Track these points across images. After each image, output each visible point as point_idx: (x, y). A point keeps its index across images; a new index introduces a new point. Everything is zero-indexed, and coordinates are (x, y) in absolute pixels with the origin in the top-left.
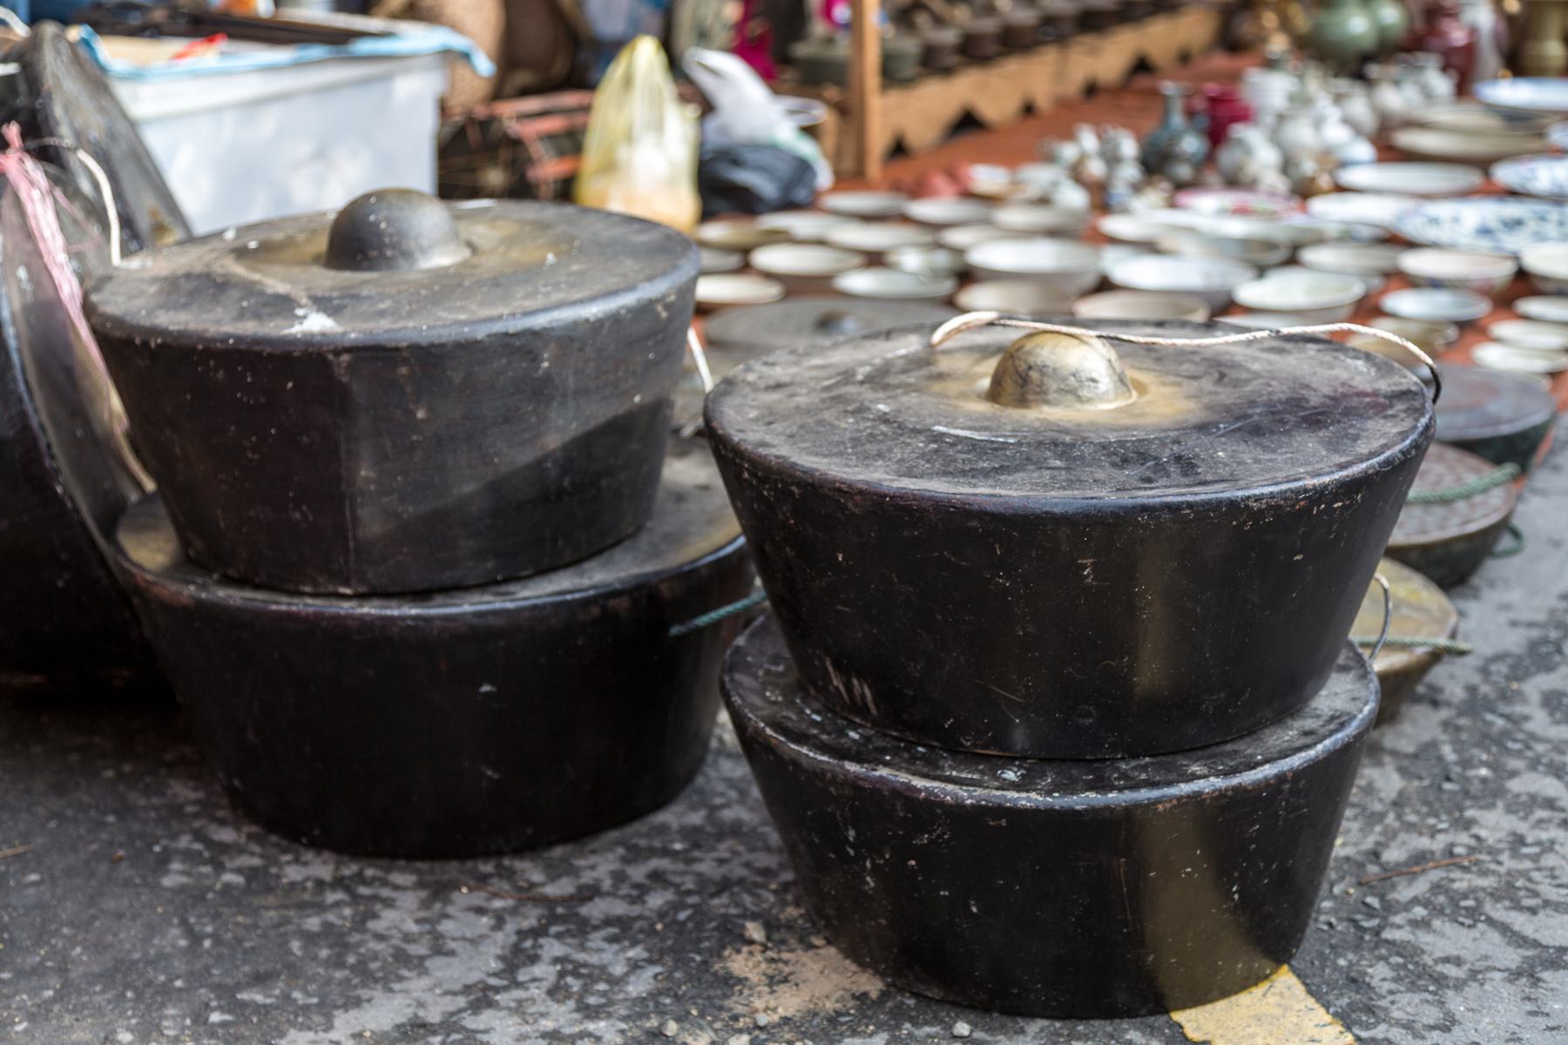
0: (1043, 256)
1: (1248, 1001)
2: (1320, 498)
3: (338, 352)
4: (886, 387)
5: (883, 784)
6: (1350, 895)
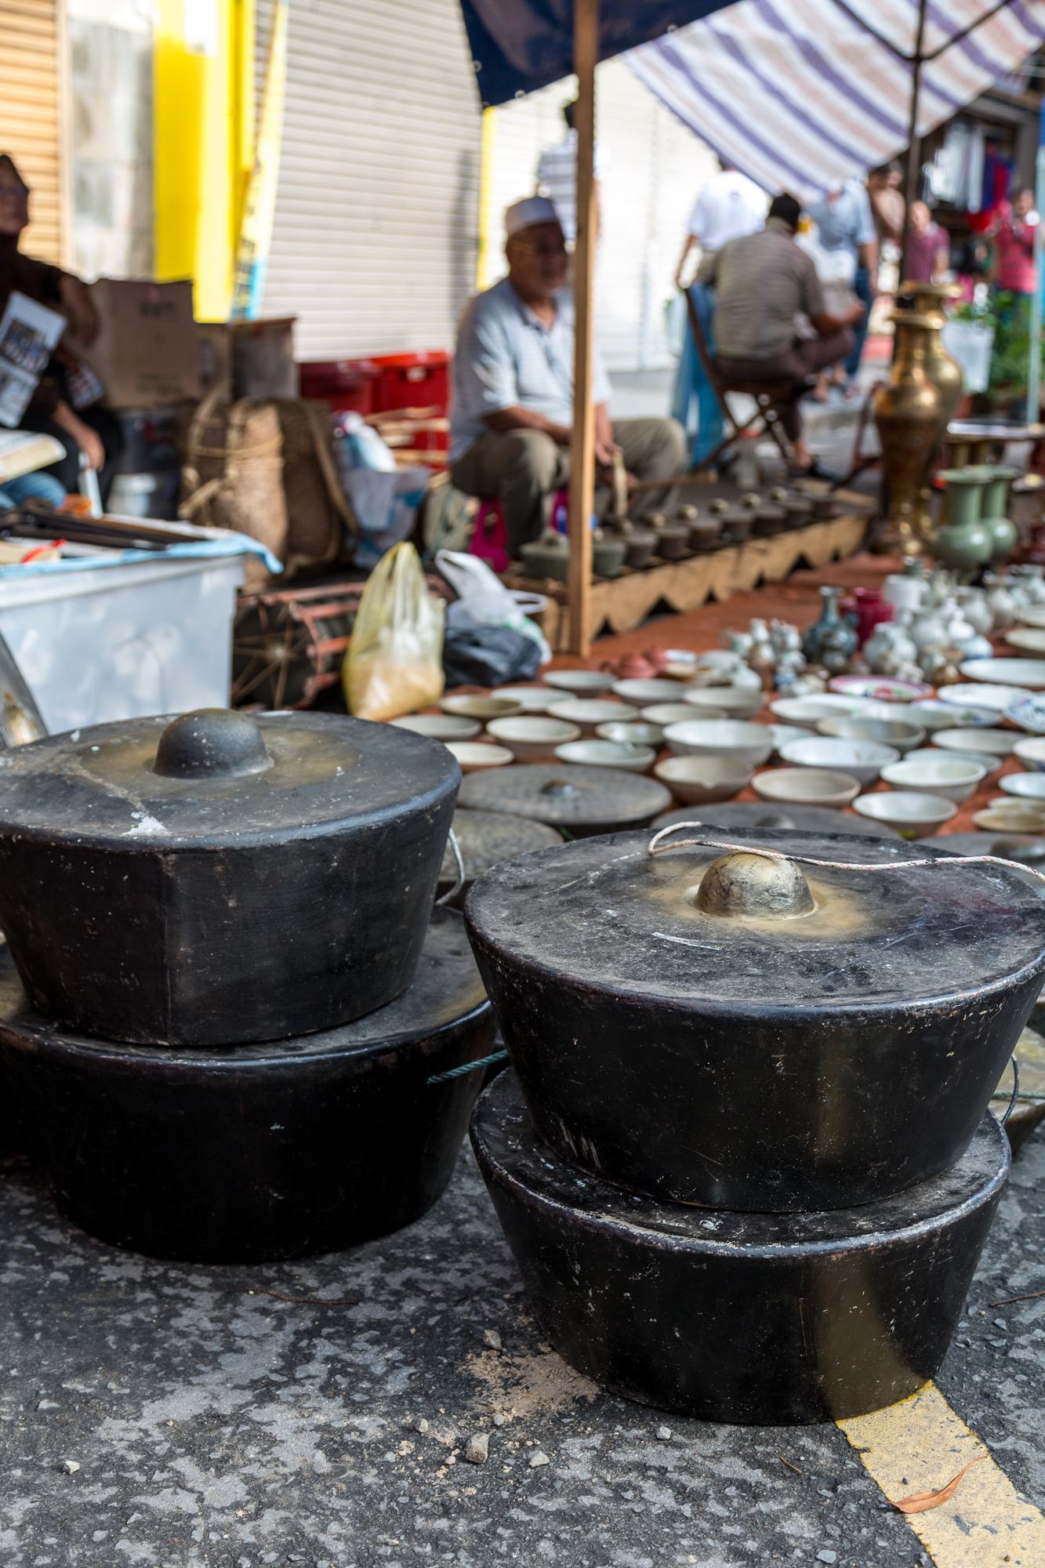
0: (723, 734)
1: (900, 1412)
2: (969, 1007)
3: (166, 853)
4: (612, 893)
5: (606, 1229)
6: (983, 1316)
